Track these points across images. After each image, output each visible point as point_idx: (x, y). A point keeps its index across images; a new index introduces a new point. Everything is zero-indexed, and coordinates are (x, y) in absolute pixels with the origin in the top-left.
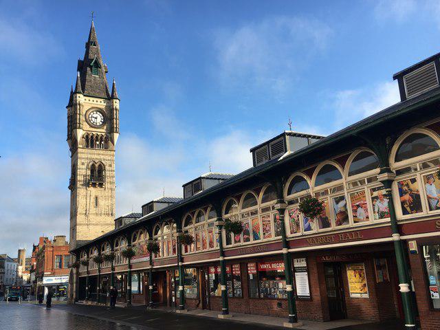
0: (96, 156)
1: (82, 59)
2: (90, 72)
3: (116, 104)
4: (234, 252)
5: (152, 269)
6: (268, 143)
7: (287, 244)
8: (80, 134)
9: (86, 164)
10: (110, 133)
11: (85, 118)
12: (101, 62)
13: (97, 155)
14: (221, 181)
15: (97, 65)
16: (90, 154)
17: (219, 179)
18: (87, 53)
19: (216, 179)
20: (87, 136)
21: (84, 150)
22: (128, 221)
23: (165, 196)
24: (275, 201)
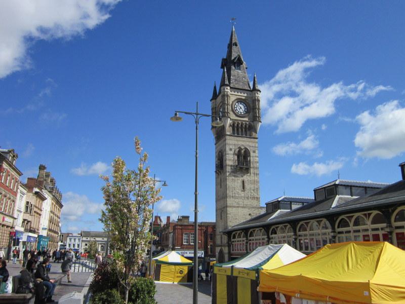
2: (234, 68)
9: (233, 150)
10: (253, 122)
13: (243, 142)
20: (233, 124)
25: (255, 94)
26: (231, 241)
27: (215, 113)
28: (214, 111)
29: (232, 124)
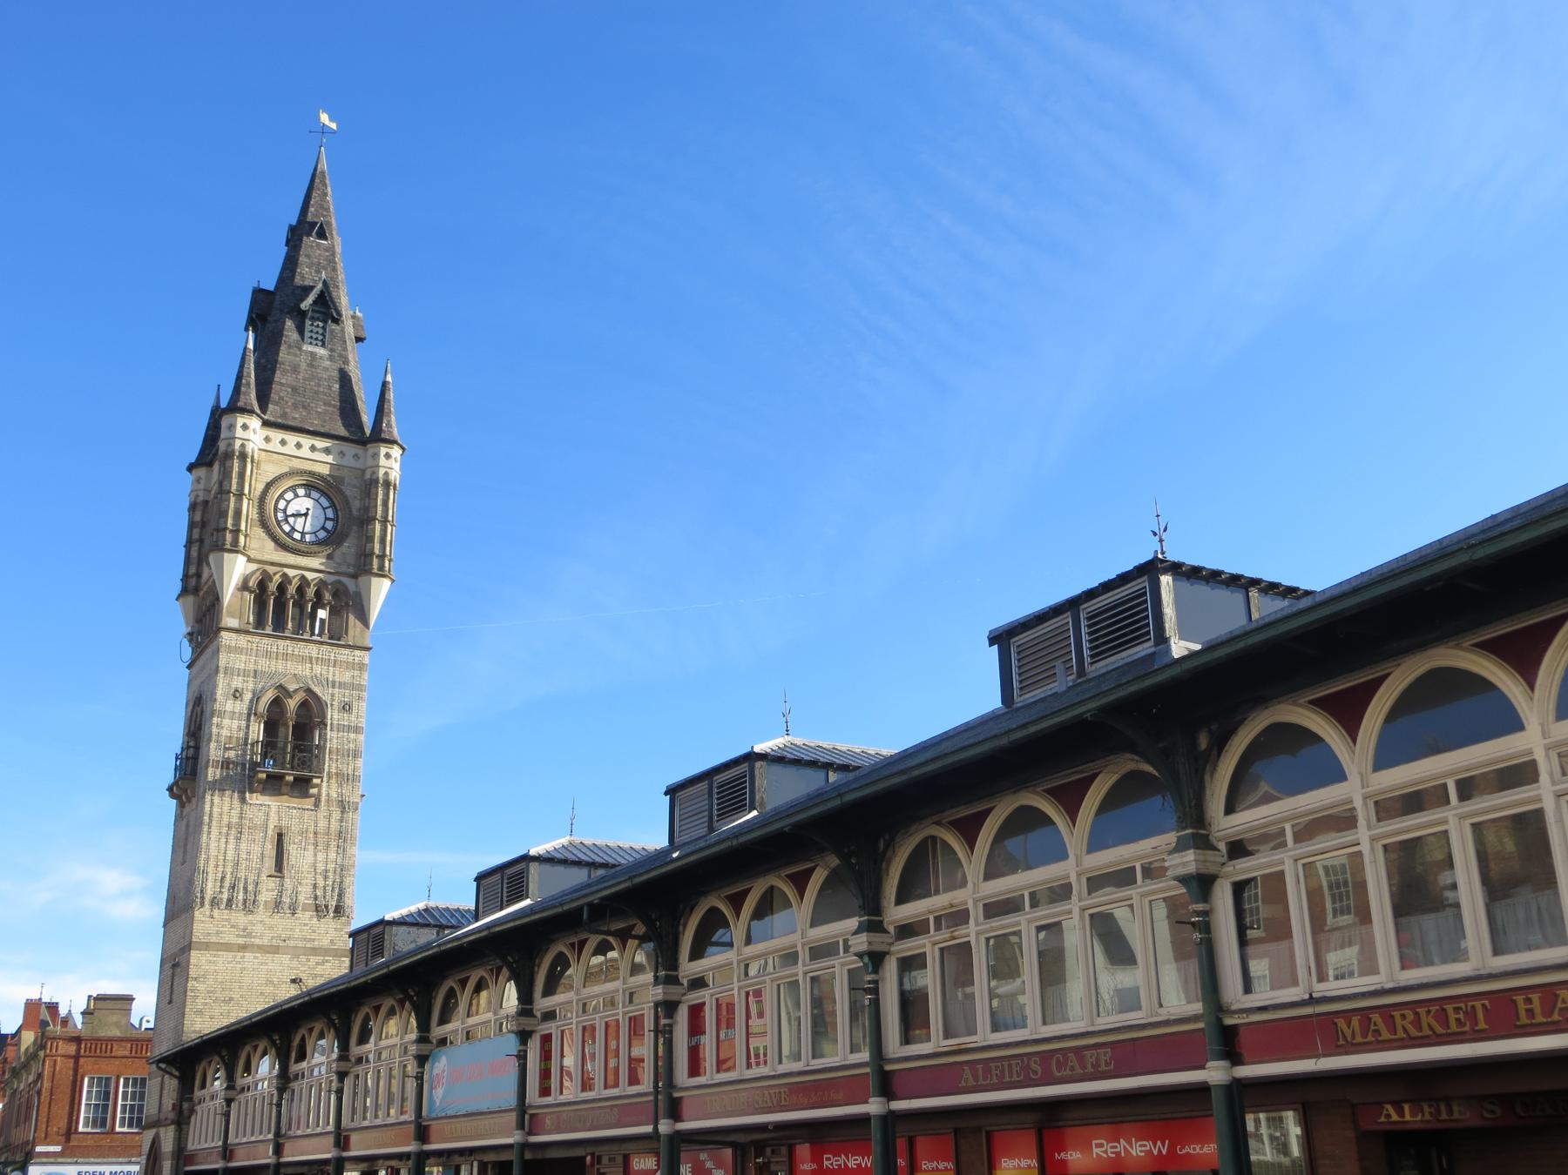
0: (294, 668)
1: (270, 285)
2: (295, 336)
3: (391, 463)
4: (941, 1076)
5: (525, 1146)
6: (1073, 604)
7: (1230, 1044)
8: (235, 570)
9: (248, 696)
12: (343, 300)
14: (833, 777)
15: (326, 308)
16: (268, 654)
17: (828, 766)
18: (291, 263)
19: (813, 764)
20: (262, 585)
21: (242, 640)
22: (405, 943)
23: (577, 839)
24: (1171, 838)
25: (376, 456)
26: (191, 1099)
27: (204, 524)
28: (198, 517)
29: (252, 583)
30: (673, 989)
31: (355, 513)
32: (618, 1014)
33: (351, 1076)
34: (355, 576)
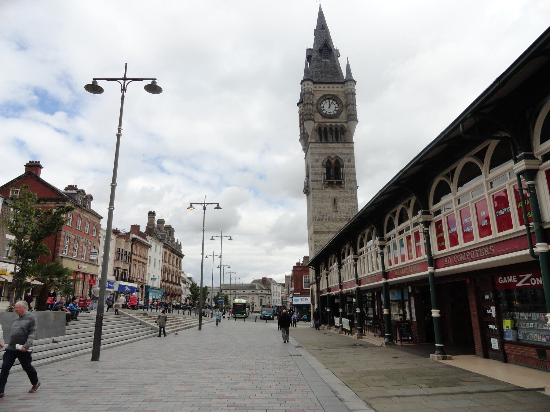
11: (317, 108)
30: (531, 162)
31: (344, 104)
32: (484, 196)
33: (359, 260)
34: (346, 122)
